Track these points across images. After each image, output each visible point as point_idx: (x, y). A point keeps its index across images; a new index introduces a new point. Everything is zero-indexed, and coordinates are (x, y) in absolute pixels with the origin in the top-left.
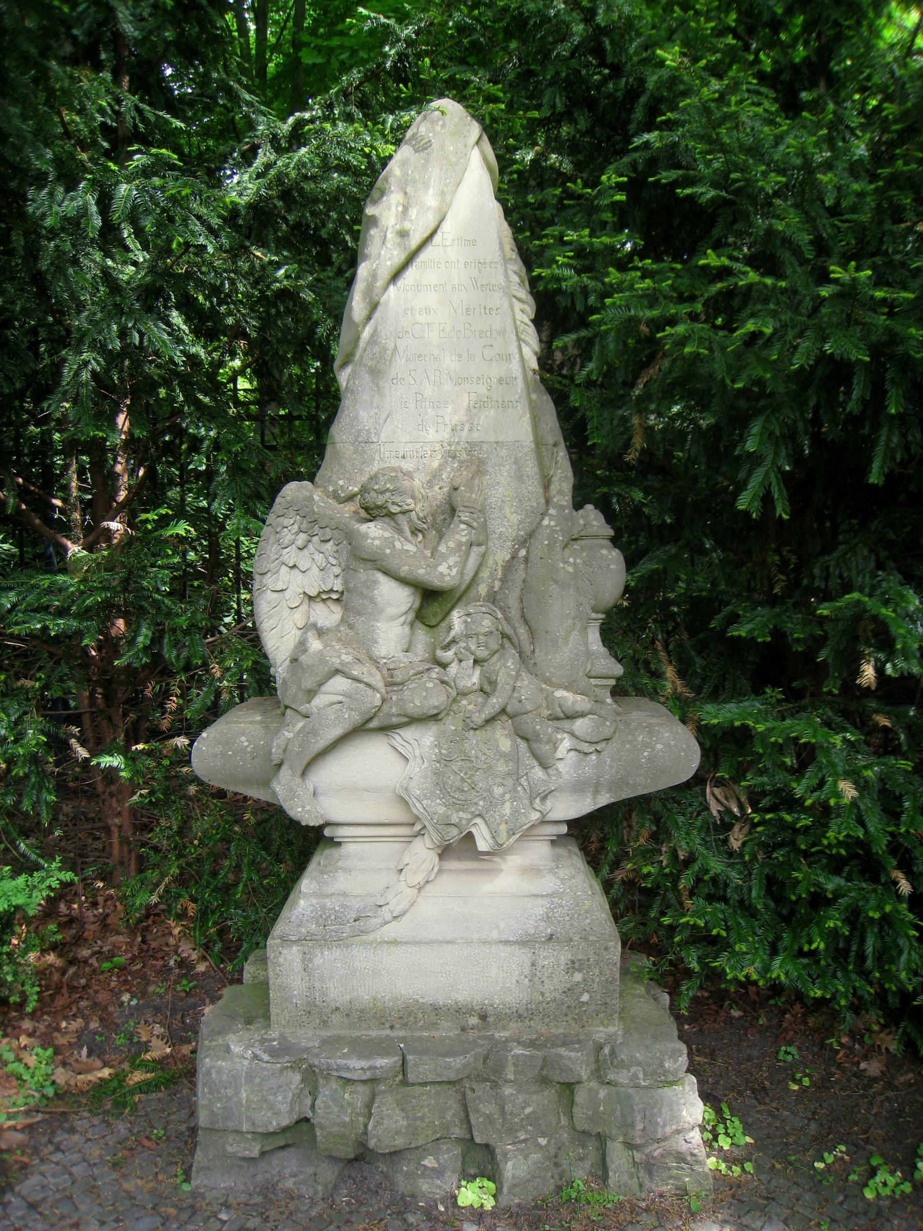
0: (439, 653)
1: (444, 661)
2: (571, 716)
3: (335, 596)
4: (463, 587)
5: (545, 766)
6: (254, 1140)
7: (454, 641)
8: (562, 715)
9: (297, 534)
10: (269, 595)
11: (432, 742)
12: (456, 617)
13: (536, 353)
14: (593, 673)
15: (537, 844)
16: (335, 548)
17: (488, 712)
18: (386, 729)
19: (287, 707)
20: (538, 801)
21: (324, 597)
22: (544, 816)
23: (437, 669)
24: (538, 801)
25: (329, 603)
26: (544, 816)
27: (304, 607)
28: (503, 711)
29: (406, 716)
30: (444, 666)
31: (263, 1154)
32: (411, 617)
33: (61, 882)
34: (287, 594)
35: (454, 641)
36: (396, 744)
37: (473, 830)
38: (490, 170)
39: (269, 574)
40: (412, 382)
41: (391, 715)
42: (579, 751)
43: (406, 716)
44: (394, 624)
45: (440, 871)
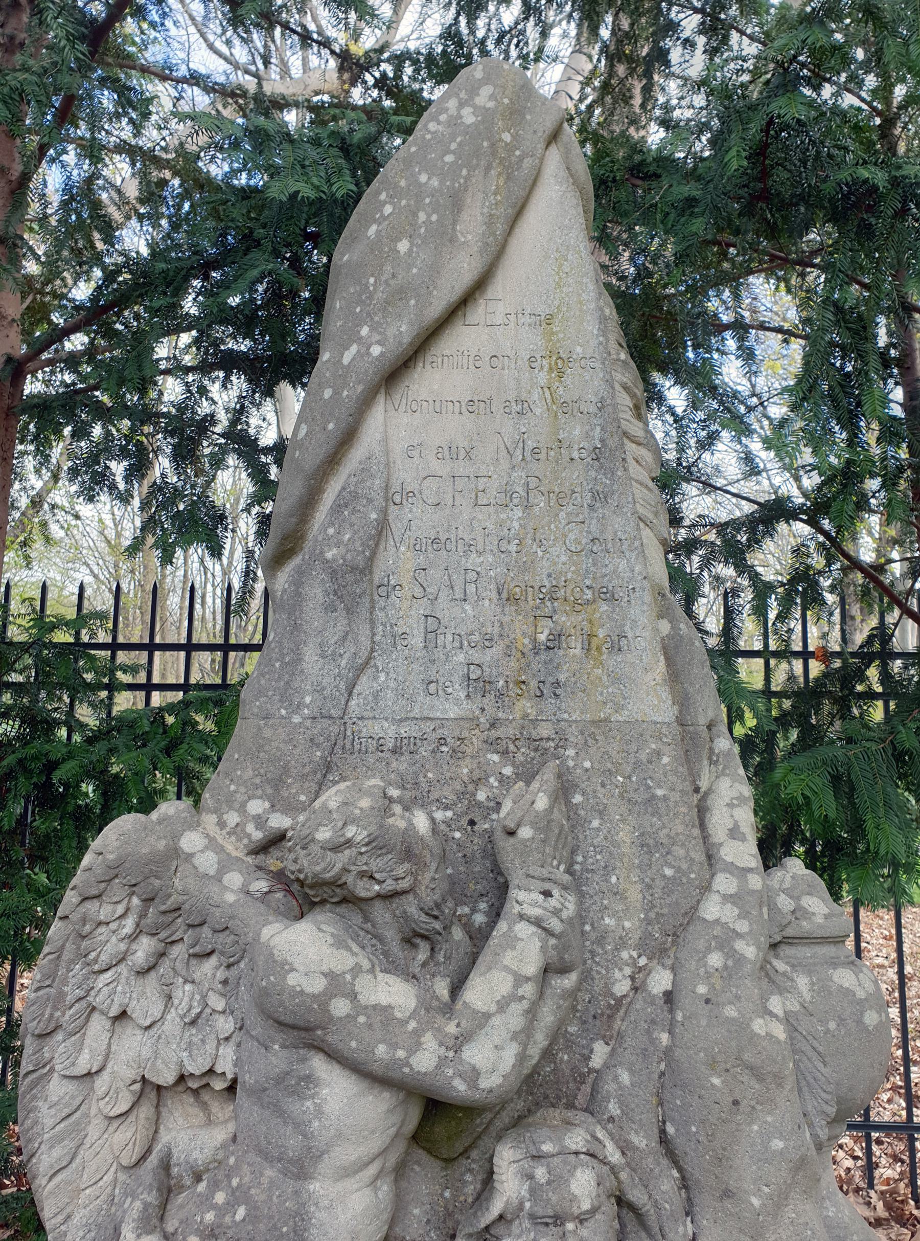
9: (133, 938)
10: (57, 1088)
16: (221, 974)
33: (330, 608)
34: (101, 1084)
39: (59, 1036)
40: (418, 592)
44: (351, 1184)
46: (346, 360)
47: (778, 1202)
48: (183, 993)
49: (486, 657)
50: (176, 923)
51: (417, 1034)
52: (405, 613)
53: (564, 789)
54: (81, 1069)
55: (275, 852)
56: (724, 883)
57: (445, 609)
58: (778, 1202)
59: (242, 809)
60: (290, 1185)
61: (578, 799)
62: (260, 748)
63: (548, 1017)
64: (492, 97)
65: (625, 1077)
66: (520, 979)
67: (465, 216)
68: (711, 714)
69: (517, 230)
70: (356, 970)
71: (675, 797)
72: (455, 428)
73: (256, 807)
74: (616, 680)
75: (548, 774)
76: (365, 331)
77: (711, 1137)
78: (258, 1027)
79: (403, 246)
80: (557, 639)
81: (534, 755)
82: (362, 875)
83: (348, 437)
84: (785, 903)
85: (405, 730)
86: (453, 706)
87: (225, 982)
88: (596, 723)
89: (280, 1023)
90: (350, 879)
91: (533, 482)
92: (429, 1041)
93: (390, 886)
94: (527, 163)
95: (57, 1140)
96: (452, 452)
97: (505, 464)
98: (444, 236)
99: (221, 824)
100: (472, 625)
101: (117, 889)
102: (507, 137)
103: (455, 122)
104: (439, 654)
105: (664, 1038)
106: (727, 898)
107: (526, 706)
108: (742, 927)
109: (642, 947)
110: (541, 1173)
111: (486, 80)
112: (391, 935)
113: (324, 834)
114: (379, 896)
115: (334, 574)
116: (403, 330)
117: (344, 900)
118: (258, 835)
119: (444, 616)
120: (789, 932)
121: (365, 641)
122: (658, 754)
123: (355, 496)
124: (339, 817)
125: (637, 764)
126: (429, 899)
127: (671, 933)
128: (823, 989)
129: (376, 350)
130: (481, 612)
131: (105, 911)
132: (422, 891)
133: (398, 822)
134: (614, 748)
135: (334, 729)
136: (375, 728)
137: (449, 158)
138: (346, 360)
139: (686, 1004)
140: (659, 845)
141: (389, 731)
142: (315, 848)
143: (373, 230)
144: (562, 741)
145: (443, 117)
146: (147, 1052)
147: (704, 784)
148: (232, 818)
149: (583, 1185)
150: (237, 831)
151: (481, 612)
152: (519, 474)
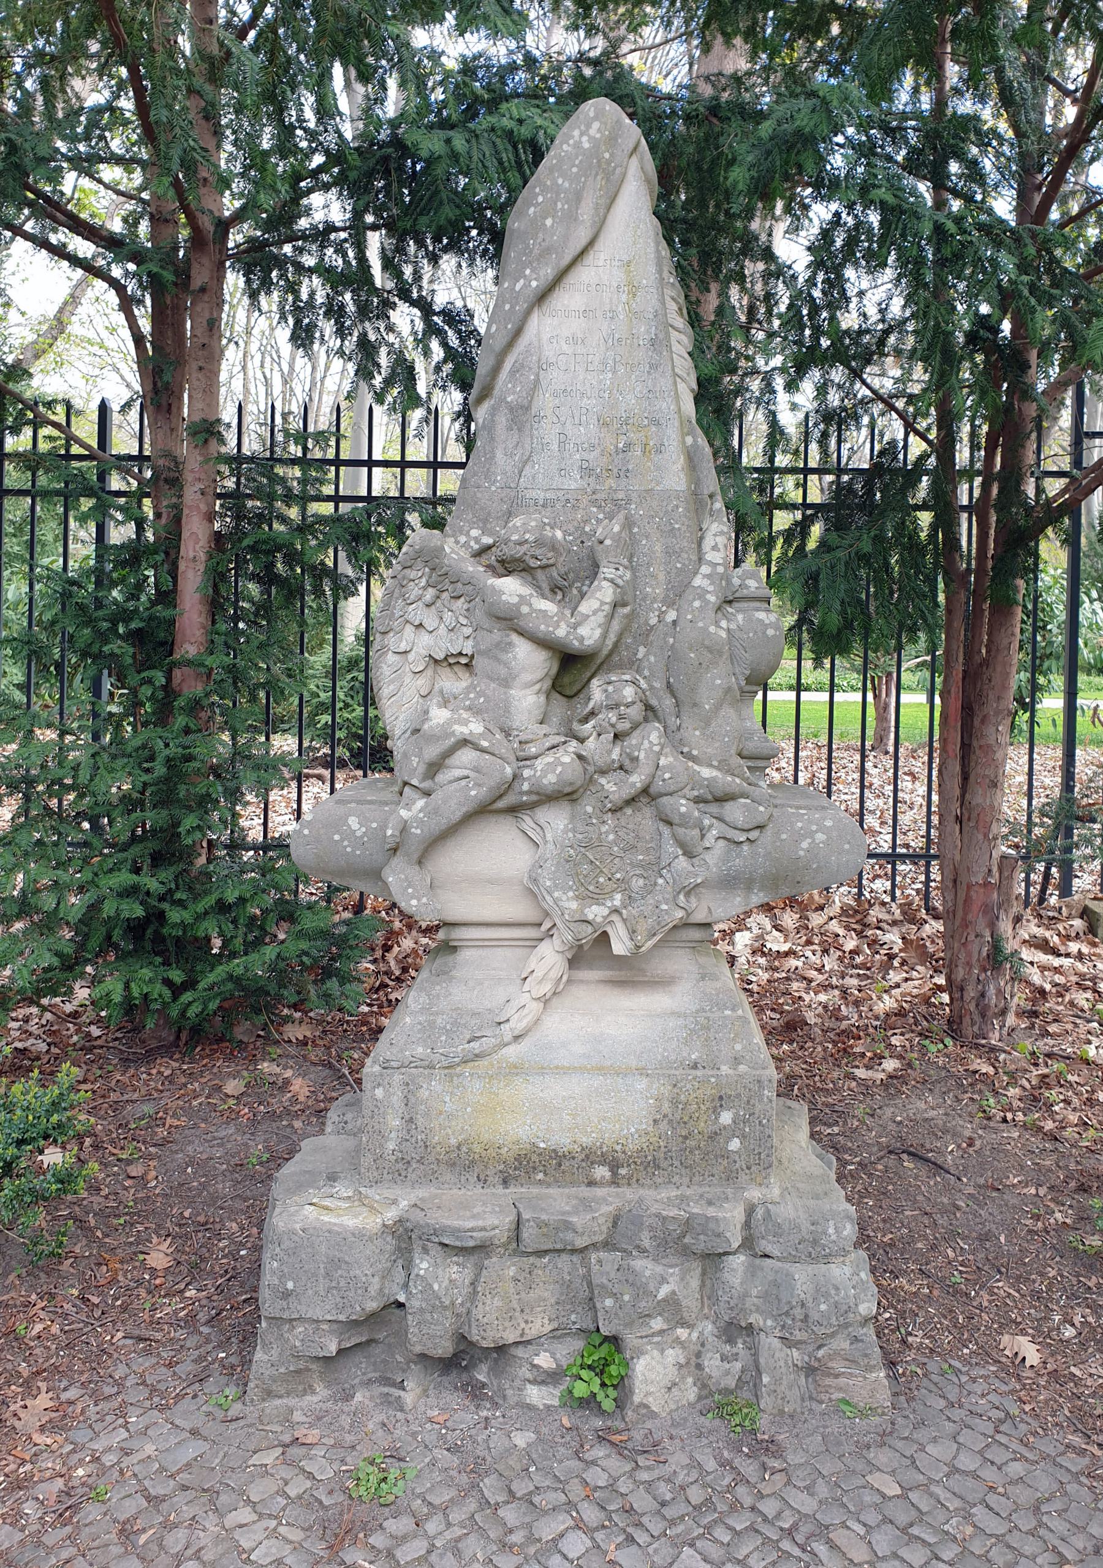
0: (576, 726)
1: (581, 735)
2: (722, 799)
3: (464, 661)
4: (605, 652)
5: (689, 854)
6: (331, 1332)
7: (593, 714)
8: (710, 797)
9: (424, 588)
10: (391, 658)
11: (566, 826)
12: (597, 691)
13: (692, 391)
14: (745, 753)
15: (680, 952)
16: (466, 606)
17: (627, 793)
18: (513, 810)
19: (405, 784)
20: (682, 897)
21: (452, 661)
22: (688, 915)
23: (574, 743)
24: (682, 897)
25: (456, 668)
26: (688, 915)
27: (429, 672)
28: (645, 791)
29: (538, 793)
30: (582, 741)
31: (340, 1352)
32: (548, 683)
34: (411, 657)
35: (593, 714)
36: (525, 827)
37: (609, 929)
38: (648, 181)
40: (555, 420)
41: (522, 793)
42: (728, 840)
43: (538, 793)
44: (528, 691)
45: (569, 981)
46: (518, 288)
47: (717, 707)
48: (448, 616)
49: (591, 456)
50: (446, 582)
51: (558, 622)
52: (548, 431)
53: (628, 524)
54: (402, 649)
55: (484, 556)
56: (705, 569)
57: (569, 430)
58: (717, 707)
59: (468, 534)
60: (502, 690)
61: (636, 530)
62: (476, 503)
63: (616, 626)
64: (599, 130)
65: (652, 659)
66: (603, 603)
67: (583, 204)
68: (712, 489)
69: (610, 217)
70: (531, 595)
71: (684, 528)
72: (576, 326)
73: (475, 533)
74: (658, 469)
75: (621, 516)
76: (528, 272)
77: (689, 680)
78: (486, 623)
79: (549, 222)
80: (629, 445)
81: (614, 506)
82: (533, 556)
83: (518, 332)
84: (736, 581)
85: (549, 495)
86: (574, 482)
87: (468, 610)
88: (647, 491)
89: (498, 618)
90: (527, 558)
91: (618, 358)
92: (563, 625)
93: (545, 561)
94: (618, 171)
95: (392, 682)
96: (573, 340)
97: (603, 348)
98: (571, 217)
99: (457, 542)
100: (584, 439)
101: (419, 564)
102: (607, 155)
103: (578, 145)
104: (566, 454)
105: (671, 640)
106: (705, 576)
107: (611, 482)
108: (711, 588)
109: (664, 602)
110: (610, 688)
111: (596, 118)
112: (545, 586)
113: (515, 537)
114: (540, 567)
115: (511, 410)
116: (548, 272)
117: (524, 570)
118: (476, 547)
119: (569, 433)
120: (737, 595)
121: (527, 447)
122: (677, 507)
123: (522, 366)
124: (522, 529)
125: (666, 512)
126: (563, 570)
127: (678, 593)
128: (749, 620)
129: (534, 284)
130: (589, 431)
131: (413, 574)
132: (559, 566)
133: (548, 532)
134: (655, 504)
135: (513, 494)
136: (533, 494)
137: (575, 170)
138: (518, 288)
139: (681, 623)
140: (675, 552)
141: (541, 495)
142: (511, 544)
143: (532, 210)
144: (629, 501)
145: (571, 142)
146: (432, 643)
147: (704, 527)
148: (463, 539)
149: (629, 692)
150: (466, 545)
151: (589, 431)
152: (610, 353)
